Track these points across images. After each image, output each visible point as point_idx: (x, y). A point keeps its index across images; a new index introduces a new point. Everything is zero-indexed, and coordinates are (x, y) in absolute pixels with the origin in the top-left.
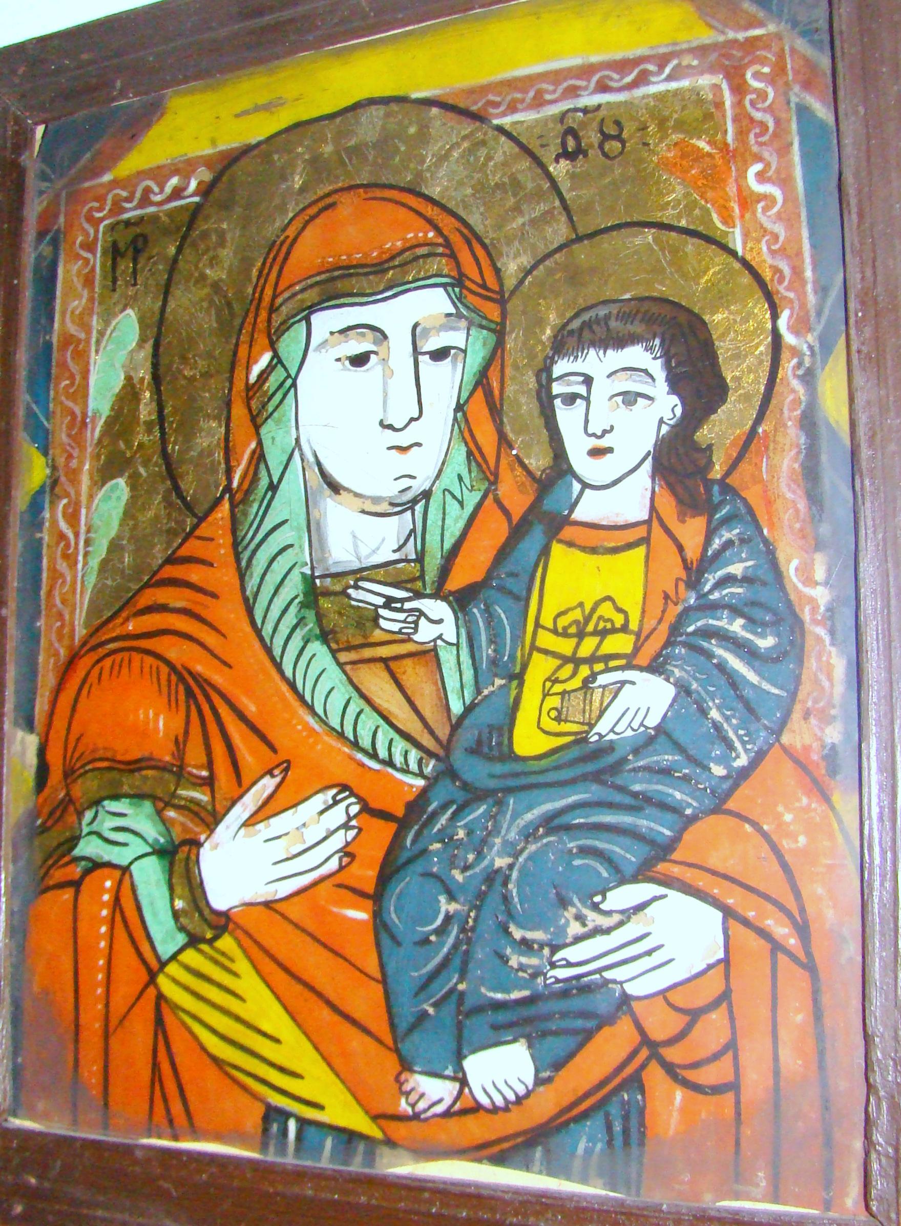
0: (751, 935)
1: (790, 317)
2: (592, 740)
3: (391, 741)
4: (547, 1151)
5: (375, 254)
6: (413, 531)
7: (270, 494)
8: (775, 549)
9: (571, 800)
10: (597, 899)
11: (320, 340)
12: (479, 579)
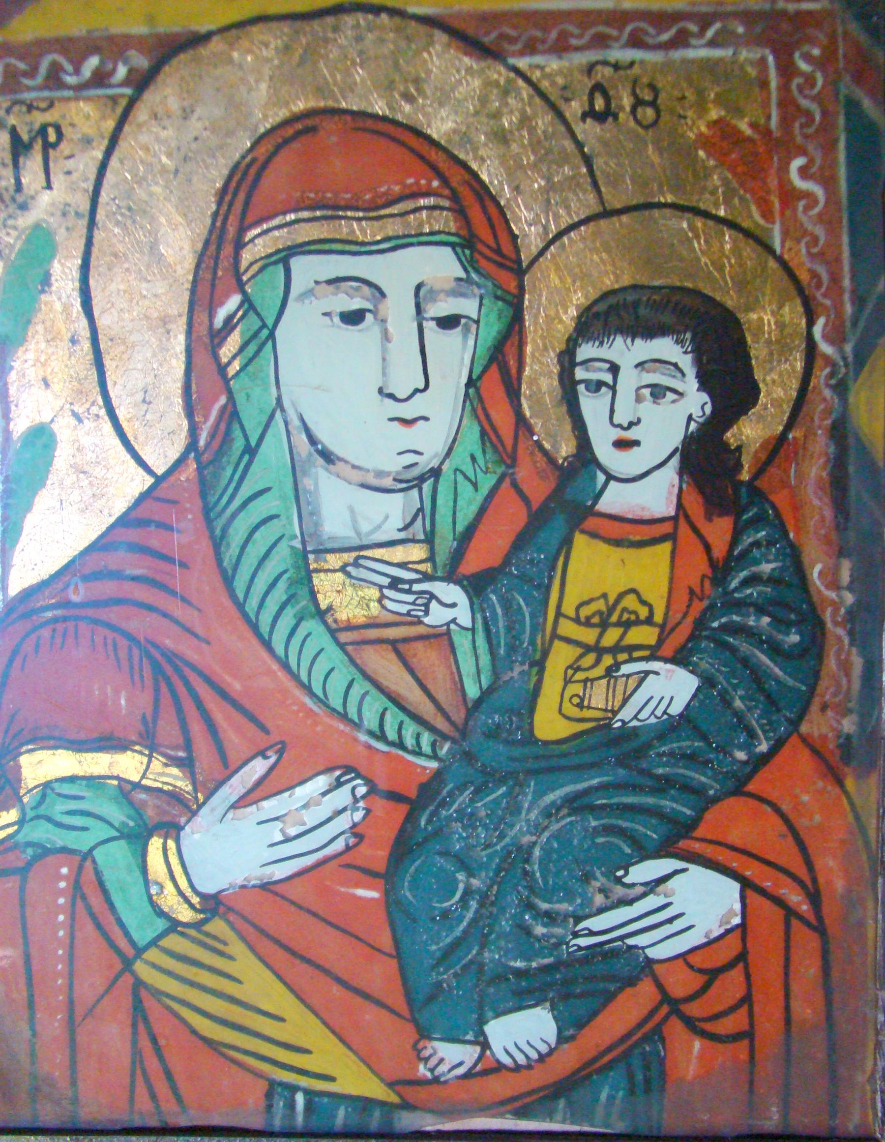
0: (767, 904)
1: (826, 325)
2: (616, 726)
3: (401, 724)
4: (570, 1104)
5: (367, 197)
6: (421, 510)
7: (246, 458)
8: (801, 553)
9: (595, 782)
10: (620, 873)
11: (302, 290)
12: (496, 565)
